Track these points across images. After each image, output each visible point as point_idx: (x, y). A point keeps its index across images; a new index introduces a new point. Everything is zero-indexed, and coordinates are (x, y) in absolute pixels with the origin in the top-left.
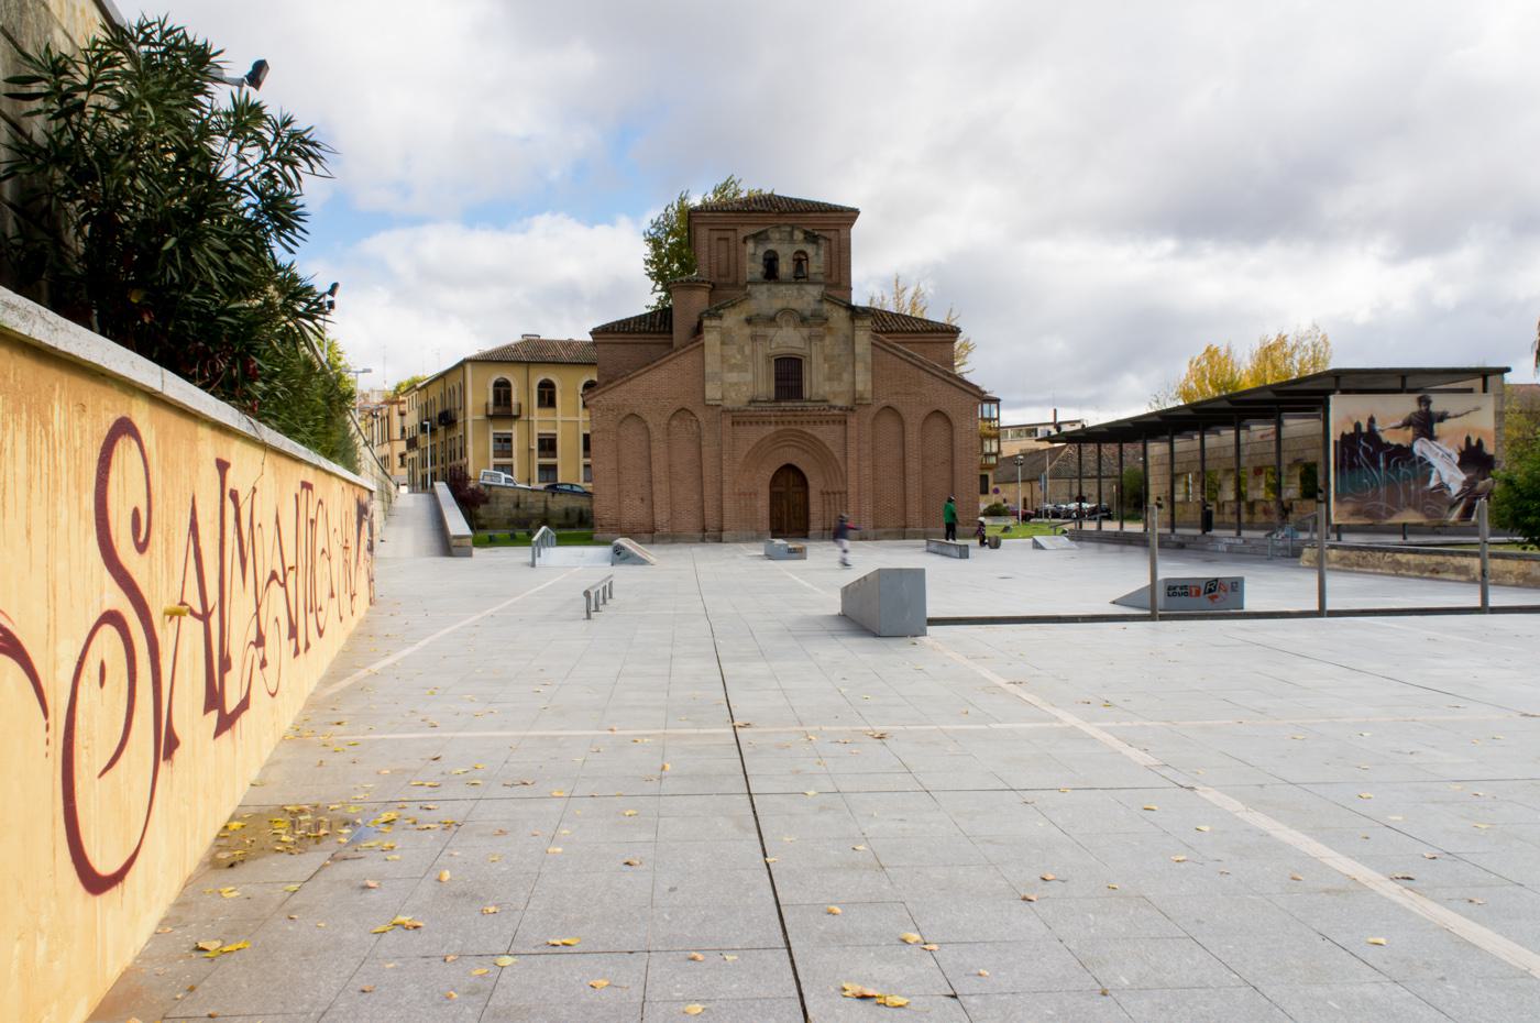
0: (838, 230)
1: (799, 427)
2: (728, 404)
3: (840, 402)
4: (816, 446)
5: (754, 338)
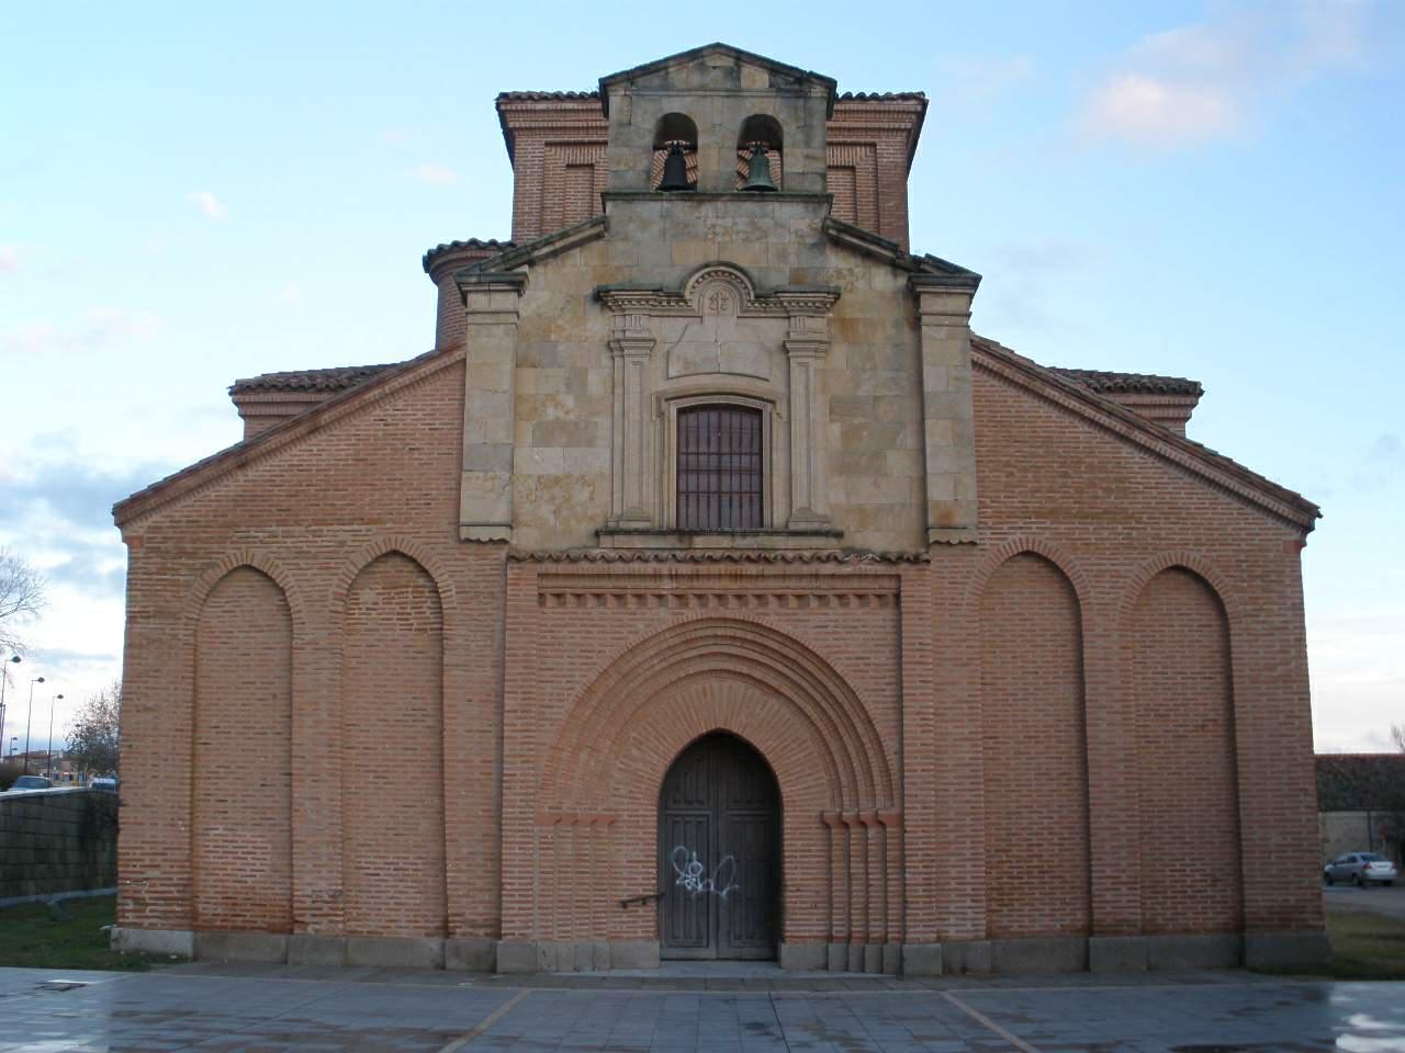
0: (873, 145)
1: (751, 612)
2: (526, 540)
3: (878, 540)
4: (808, 678)
5: (615, 346)
